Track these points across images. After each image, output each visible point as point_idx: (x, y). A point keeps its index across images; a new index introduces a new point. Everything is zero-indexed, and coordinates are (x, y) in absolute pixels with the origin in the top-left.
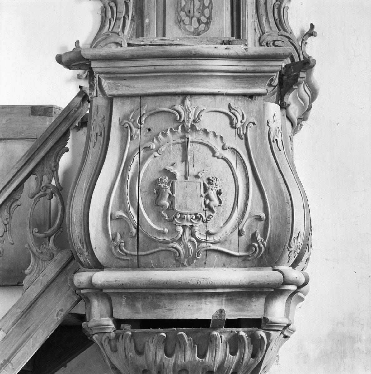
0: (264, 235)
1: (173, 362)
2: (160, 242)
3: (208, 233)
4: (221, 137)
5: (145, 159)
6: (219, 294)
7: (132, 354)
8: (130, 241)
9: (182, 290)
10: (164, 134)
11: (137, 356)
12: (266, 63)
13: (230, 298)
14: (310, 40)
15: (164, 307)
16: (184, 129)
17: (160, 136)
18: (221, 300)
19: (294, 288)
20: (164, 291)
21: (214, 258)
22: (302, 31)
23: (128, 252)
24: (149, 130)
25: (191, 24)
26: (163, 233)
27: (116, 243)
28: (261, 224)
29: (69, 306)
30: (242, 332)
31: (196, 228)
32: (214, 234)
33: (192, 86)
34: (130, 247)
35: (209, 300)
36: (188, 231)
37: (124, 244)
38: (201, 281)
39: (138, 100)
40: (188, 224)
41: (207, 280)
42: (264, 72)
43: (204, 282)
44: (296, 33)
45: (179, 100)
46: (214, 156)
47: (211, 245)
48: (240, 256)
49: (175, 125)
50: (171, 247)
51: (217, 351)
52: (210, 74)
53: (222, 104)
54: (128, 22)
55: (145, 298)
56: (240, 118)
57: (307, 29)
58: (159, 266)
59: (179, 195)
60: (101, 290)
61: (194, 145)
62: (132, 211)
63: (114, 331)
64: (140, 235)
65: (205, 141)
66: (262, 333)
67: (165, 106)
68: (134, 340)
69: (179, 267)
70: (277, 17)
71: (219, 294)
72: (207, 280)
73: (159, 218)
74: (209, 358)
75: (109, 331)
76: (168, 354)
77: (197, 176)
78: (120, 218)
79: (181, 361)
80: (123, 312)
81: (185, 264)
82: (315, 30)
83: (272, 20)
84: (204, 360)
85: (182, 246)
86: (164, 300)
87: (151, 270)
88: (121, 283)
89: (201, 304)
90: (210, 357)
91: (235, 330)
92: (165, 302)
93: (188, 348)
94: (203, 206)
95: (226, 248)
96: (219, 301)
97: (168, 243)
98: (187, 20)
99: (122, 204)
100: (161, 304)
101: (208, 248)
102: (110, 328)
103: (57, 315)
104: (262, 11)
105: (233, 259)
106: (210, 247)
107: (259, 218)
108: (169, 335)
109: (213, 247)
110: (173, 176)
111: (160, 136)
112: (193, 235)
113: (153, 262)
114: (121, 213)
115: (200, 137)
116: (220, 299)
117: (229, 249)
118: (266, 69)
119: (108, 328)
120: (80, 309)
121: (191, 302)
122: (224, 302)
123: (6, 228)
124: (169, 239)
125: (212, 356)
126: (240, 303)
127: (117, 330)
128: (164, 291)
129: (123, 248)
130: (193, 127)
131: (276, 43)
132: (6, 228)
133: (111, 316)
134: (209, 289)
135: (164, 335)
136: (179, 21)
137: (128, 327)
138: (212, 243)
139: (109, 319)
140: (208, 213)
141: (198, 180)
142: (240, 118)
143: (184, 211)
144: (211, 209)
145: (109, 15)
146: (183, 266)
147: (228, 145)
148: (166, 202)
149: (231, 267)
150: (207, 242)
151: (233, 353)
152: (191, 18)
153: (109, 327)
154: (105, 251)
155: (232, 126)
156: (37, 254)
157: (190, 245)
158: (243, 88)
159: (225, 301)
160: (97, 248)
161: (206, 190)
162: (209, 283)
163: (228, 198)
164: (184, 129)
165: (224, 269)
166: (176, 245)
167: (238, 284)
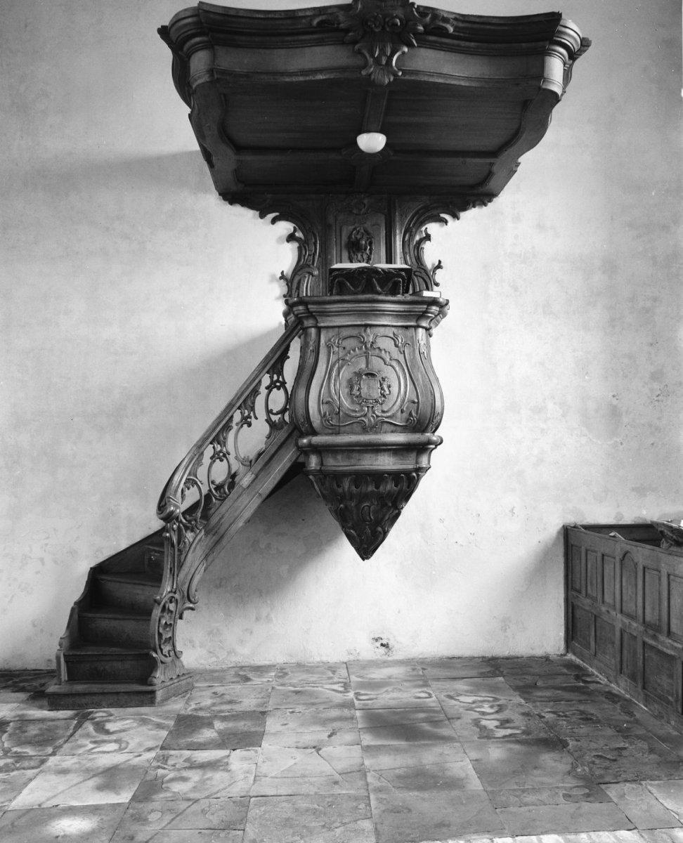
0: (417, 413)
2: (353, 417)
3: (383, 412)
4: (389, 353)
5: (342, 366)
8: (334, 416)
10: (354, 350)
14: (438, 271)
17: (352, 352)
19: (433, 446)
20: (355, 448)
22: (433, 264)
24: (344, 348)
32: (387, 412)
33: (375, 321)
36: (370, 409)
39: (337, 329)
42: (416, 312)
45: (363, 329)
46: (385, 364)
49: (361, 345)
53: (390, 332)
54: (317, 257)
56: (400, 341)
57: (437, 264)
60: (316, 448)
61: (373, 357)
64: (341, 413)
70: (416, 254)
82: (442, 264)
94: (380, 395)
107: (414, 402)
111: (352, 352)
112: (374, 413)
113: (365, 529)
120: (301, 460)
128: (355, 448)
131: (416, 273)
138: (386, 418)
140: (383, 399)
142: (400, 341)
143: (368, 397)
144: (384, 396)
151: (396, 486)
155: (396, 346)
157: (372, 419)
158: (402, 322)
161: (381, 385)
163: (395, 389)
166: (363, 419)
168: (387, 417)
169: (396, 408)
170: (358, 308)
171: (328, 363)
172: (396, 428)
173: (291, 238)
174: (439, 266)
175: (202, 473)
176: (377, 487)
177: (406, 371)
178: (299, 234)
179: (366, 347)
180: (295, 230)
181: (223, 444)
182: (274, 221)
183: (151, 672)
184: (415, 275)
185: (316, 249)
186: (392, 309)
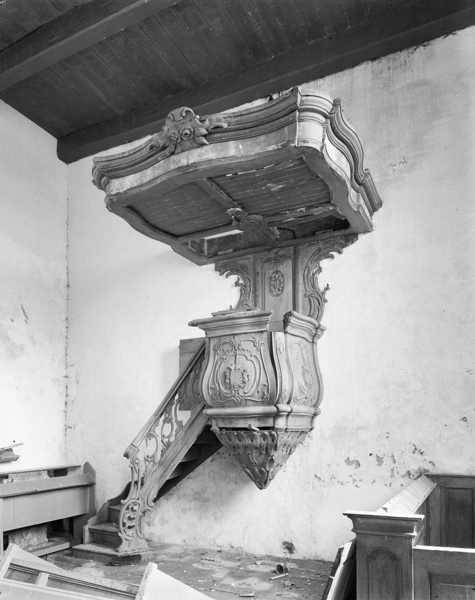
0: (268, 392)
3: (244, 393)
5: (222, 363)
6: (254, 417)
7: (228, 440)
8: (218, 396)
10: (228, 352)
12: (262, 318)
16: (235, 350)
25: (275, 291)
26: (227, 394)
28: (266, 388)
29: (206, 421)
30: (266, 432)
31: (240, 391)
35: (250, 419)
39: (219, 338)
40: (236, 390)
43: (245, 413)
44: (322, 289)
45: (232, 337)
52: (241, 325)
54: (251, 294)
56: (258, 342)
58: (230, 407)
59: (232, 378)
62: (217, 385)
65: (244, 354)
66: (274, 433)
67: (227, 339)
71: (254, 417)
73: (226, 388)
76: (240, 441)
77: (239, 369)
78: (213, 388)
79: (244, 443)
80: (222, 425)
83: (310, 285)
91: (263, 431)
92: (234, 421)
98: (273, 290)
99: (213, 383)
100: (166, 430)
104: (306, 281)
107: (265, 385)
109: (247, 398)
110: (230, 370)
114: (213, 386)
115: (242, 352)
118: (264, 320)
126: (264, 420)
130: (238, 348)
133: (217, 426)
135: (236, 433)
136: (271, 291)
137: (224, 430)
140: (244, 384)
141: (239, 371)
142: (258, 342)
144: (244, 383)
145: (243, 292)
147: (253, 354)
148: (228, 381)
150: (244, 396)
151: (264, 440)
152: (275, 289)
155: (255, 346)
157: (238, 398)
158: (259, 329)
161: (242, 375)
163: (252, 378)
164: (235, 350)
166: (233, 398)
168: (248, 397)
169: (253, 390)
170: (225, 324)
171: (214, 362)
172: (256, 403)
173: (237, 284)
174: (327, 289)
175: (158, 430)
176: (252, 441)
177: (261, 363)
178: (241, 281)
179: (235, 349)
180: (239, 280)
181: (170, 414)
182: (227, 276)
183: (119, 545)
184: (312, 297)
185: (250, 290)
186: (246, 322)
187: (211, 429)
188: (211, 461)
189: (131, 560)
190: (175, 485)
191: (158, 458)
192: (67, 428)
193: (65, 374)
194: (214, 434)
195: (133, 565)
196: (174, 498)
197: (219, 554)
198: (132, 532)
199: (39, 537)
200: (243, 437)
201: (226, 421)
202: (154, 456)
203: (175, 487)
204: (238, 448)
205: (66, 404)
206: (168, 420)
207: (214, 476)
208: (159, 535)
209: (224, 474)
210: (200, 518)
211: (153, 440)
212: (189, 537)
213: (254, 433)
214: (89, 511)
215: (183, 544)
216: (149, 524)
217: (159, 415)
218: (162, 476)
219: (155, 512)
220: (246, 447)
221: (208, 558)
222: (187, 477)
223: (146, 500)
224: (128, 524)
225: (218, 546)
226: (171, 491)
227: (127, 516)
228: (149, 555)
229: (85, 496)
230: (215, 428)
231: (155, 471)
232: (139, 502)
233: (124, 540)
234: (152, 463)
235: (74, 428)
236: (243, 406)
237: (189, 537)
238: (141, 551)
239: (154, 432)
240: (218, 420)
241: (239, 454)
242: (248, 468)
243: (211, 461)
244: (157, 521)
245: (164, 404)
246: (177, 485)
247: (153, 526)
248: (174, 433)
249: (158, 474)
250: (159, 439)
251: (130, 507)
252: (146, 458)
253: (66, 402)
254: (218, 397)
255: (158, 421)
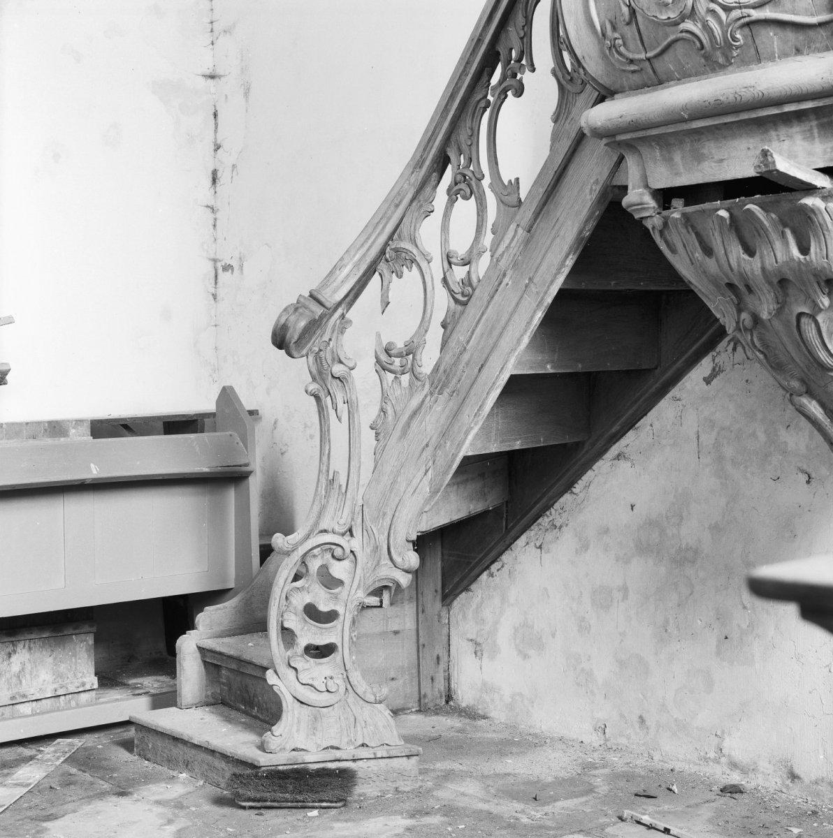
1: (759, 265)
6: (799, 116)
7: (699, 254)
9: (721, 117)
11: (706, 257)
13: (825, 120)
15: (710, 157)
18: (808, 128)
21: (771, 38)
23: (631, 56)
27: (609, 42)
29: (606, 173)
34: (632, 46)
35: (783, 131)
37: (620, 42)
38: (742, 94)
41: (752, 89)
43: (747, 95)
47: (752, 12)
48: (821, 25)
50: (682, 32)
51: (827, 237)
55: (681, 142)
58: (685, 75)
63: (659, 213)
68: (692, 227)
69: (715, 69)
72: (752, 89)
74: (816, 253)
75: (648, 215)
76: (751, 253)
79: (770, 263)
80: (664, 178)
81: (721, 60)
84: (807, 257)
85: (699, 25)
86: (707, 143)
87: (677, 84)
88: (629, 119)
89: (770, 141)
90: (818, 250)
92: (710, 147)
93: (774, 236)
95: (786, 12)
96: (805, 131)
97: (676, 24)
100: (705, 151)
101: (747, 19)
102: (649, 208)
103: (591, 194)
105: (811, 33)
106: (749, 16)
108: (736, 212)
116: (805, 126)
117: (794, 14)
119: (644, 208)
121: (751, 141)
122: (816, 131)
123: (523, 44)
124: (676, 16)
125: (821, 250)
127: (664, 210)
129: (622, 49)
132: (523, 44)
133: (647, 186)
134: (768, 108)
135: (723, 213)
137: (677, 203)
139: (645, 191)
146: (722, 67)
149: (814, 52)
153: (645, 206)
154: (600, 61)
156: (564, 82)
159: (818, 129)
160: (587, 58)
162: (756, 95)
165: (799, 58)
166: (688, 25)
167: (818, 88)
175: (428, 233)
176: (804, 250)
187: (625, 202)
188: (708, 381)
189: (312, 790)
190: (569, 487)
191: (429, 358)
192: (220, 268)
193: (207, 69)
194: (639, 223)
195: (315, 813)
196: (564, 545)
197: (726, 800)
198: (328, 673)
199: (63, 667)
200: (760, 230)
201: (677, 157)
202: (411, 350)
203: (567, 498)
204: (749, 289)
205: (214, 181)
206: (466, 186)
207: (717, 445)
208: (213, 698)
209: (762, 437)
210: (663, 634)
211: (411, 275)
212: (622, 716)
213: (809, 201)
214: (236, 579)
215: (594, 739)
216: (478, 648)
217: (428, 163)
218: (444, 434)
219: (497, 601)
220: (782, 283)
221: (646, 819)
222: (614, 450)
223: (383, 538)
224: (309, 634)
225: (734, 765)
226: (553, 514)
227: (300, 601)
228: (401, 774)
229: (217, 516)
230: (638, 198)
231: (415, 413)
232: (355, 544)
233: (288, 702)
234: (405, 379)
235: (241, 267)
236: (745, 63)
237: (622, 716)
238: (364, 753)
239: (414, 242)
240: (644, 150)
241: (756, 319)
242: (810, 393)
243: (708, 381)
244: (504, 636)
245: (446, 109)
246: (578, 488)
247: (492, 658)
248: (488, 239)
249: (430, 424)
250: (436, 269)
251: (314, 565)
252: (384, 357)
253: (215, 173)
254: (630, 32)
255: (428, 189)
